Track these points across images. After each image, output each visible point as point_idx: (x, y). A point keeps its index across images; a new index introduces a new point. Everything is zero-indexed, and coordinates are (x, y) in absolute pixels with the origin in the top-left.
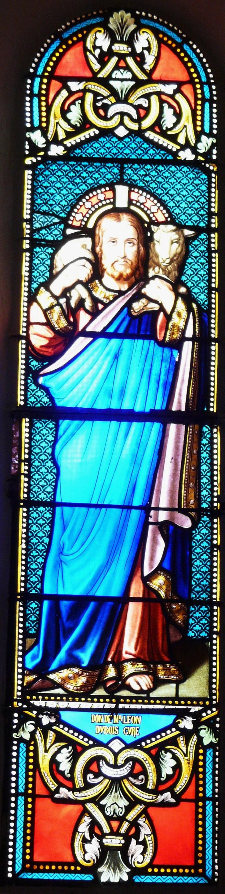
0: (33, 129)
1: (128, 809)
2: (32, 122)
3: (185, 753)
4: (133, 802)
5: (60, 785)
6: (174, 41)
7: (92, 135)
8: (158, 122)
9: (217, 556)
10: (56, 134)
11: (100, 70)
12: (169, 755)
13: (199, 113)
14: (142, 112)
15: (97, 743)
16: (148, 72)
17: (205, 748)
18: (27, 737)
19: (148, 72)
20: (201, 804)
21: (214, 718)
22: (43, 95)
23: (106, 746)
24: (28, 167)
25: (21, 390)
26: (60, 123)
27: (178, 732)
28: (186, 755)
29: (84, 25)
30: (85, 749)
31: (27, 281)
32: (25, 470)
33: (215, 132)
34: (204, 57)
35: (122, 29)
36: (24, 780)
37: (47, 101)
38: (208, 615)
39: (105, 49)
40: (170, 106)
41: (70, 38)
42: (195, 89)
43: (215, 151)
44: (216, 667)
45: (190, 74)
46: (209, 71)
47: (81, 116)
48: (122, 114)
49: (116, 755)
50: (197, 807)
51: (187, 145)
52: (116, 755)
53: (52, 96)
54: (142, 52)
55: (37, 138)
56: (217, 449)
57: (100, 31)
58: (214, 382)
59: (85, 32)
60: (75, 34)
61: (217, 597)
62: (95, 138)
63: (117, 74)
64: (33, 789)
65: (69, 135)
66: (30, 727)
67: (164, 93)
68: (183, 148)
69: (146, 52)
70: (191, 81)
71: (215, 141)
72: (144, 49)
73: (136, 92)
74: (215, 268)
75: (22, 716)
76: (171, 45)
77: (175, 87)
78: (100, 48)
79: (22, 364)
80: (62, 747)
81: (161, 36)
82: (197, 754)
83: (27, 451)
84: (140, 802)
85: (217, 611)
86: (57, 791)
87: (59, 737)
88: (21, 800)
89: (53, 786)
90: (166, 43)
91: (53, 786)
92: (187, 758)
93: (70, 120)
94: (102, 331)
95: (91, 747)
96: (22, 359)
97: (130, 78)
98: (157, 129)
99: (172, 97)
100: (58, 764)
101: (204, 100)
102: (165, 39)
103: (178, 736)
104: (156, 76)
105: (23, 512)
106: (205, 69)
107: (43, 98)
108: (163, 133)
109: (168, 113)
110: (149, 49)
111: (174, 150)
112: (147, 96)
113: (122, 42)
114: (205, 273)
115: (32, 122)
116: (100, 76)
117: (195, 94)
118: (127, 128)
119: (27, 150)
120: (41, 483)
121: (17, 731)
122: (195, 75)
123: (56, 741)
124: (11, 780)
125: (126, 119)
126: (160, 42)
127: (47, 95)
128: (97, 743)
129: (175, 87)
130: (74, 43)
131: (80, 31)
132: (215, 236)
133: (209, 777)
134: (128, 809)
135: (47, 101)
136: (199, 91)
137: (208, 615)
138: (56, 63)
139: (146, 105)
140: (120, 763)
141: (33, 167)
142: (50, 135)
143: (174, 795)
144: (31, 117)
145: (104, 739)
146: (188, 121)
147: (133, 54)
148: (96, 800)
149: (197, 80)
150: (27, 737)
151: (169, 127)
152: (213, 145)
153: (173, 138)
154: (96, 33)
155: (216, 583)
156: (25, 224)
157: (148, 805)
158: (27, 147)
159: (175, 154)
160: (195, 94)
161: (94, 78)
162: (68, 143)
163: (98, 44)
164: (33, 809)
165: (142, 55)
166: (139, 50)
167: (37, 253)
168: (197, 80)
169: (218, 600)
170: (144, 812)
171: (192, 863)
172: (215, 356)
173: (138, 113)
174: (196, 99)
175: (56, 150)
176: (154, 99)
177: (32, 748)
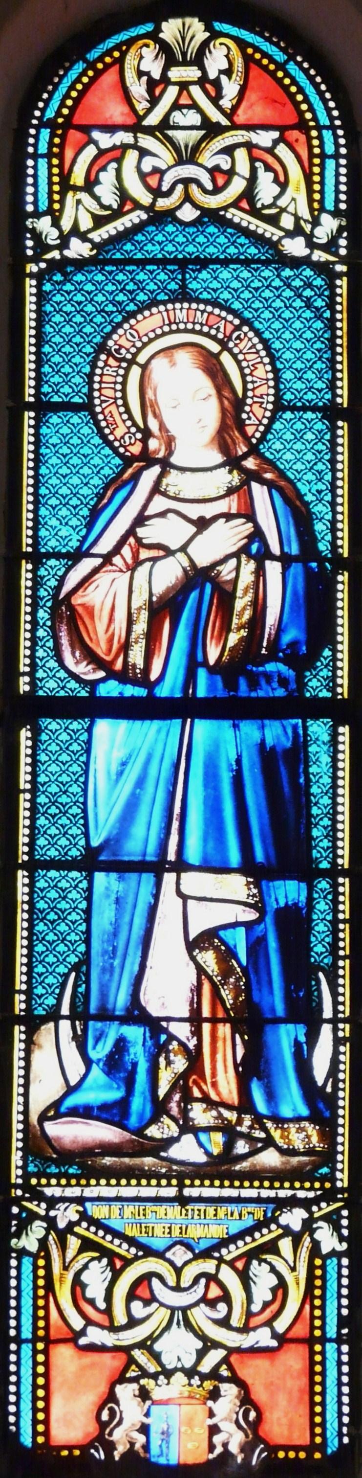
0: (37, 215)
1: (201, 1354)
2: (35, 203)
3: (292, 1265)
4: (209, 1344)
5: (89, 1322)
6: (272, 60)
7: (137, 221)
8: (249, 194)
9: (344, 968)
10: (76, 225)
11: (149, 111)
12: (265, 1267)
13: (317, 178)
14: (220, 181)
15: (149, 1252)
16: (229, 111)
17: (324, 1258)
18: (33, 1247)
19: (229, 111)
20: (318, 1348)
21: (338, 1210)
22: (55, 155)
23: (160, 1255)
24: (32, 275)
25: (26, 622)
26: (83, 200)
27: (280, 1231)
28: (293, 1269)
29: (123, 36)
30: (127, 1263)
31: (34, 362)
32: (17, 1177)
33: (343, 206)
34: (322, 83)
35: (183, 39)
36: (69, 74)
37: (61, 166)
38: (326, 336)
39: (156, 75)
40: (268, 168)
41: (100, 59)
42: (309, 139)
43: (343, 242)
44: (343, 1004)
45: (301, 113)
46: (332, 104)
47: (116, 188)
48: (186, 182)
49: (178, 1271)
50: (312, 1353)
51: (297, 231)
52: (178, 1271)
53: (69, 154)
54: (218, 78)
55: (44, 225)
56: (343, 778)
57: (147, 46)
58: (344, 1099)
59: (124, 48)
60: (109, 53)
61: (344, 862)
62: (138, 228)
63: (177, 117)
64: (47, 1328)
65: (99, 222)
66: (38, 1229)
67: (257, 146)
68: (290, 234)
69: (224, 79)
70: (302, 126)
71: (344, 223)
72: (221, 72)
73: (211, 144)
74: (344, 940)
75: (24, 1215)
76: (267, 66)
77: (276, 135)
78: (148, 74)
79: (31, 311)
80: (93, 1259)
81: (250, 51)
82: (311, 1267)
83: (24, 969)
84: (217, 1345)
85: (342, 428)
86: (83, 1333)
87: (87, 1245)
88: (26, 1349)
89: (77, 1323)
90: (258, 63)
91: (77, 1323)
92: (295, 1274)
93: (99, 197)
94: (161, 122)
95: (136, 1258)
96: (28, 528)
97: (199, 124)
98: (245, 205)
99: (270, 151)
100: (84, 1286)
101: (323, 156)
102: (258, 56)
103: (280, 1237)
104: (241, 117)
105: (20, 1032)
106: (325, 101)
107: (55, 161)
108: (255, 212)
109: (265, 179)
110: (228, 72)
111: (275, 238)
112: (229, 151)
113: (185, 63)
114: (324, 386)
115: (35, 203)
116: (146, 123)
117: (310, 147)
118: (195, 206)
119: (29, 185)
120: (74, 340)
121: (18, 1235)
122: (308, 116)
123: (81, 1251)
124: (7, 1410)
125: (194, 189)
126: (248, 60)
127: (61, 156)
128: (149, 1252)
129: (276, 135)
130: (107, 67)
131: (117, 47)
132: (345, 885)
133: (332, 1285)
134: (201, 1354)
135: (61, 166)
136: (316, 142)
137: (326, 293)
138: (77, 101)
139: (226, 166)
140: (184, 1284)
141: (40, 277)
142: (66, 224)
143: (275, 1335)
144: (35, 194)
145: (158, 1244)
146: (298, 189)
147: (203, 81)
148: (146, 1345)
149: (312, 124)
150: (33, 1247)
151: (266, 204)
152: (340, 229)
153: (273, 220)
154: (141, 48)
155: (341, 379)
156: (27, 280)
157: (231, 1351)
158: (30, 243)
159: (274, 245)
160: (310, 147)
161: (137, 127)
162: (96, 236)
163: (143, 68)
164: (46, 1364)
165: (217, 83)
166: (212, 75)
167: (41, 680)
168: (312, 124)
169: (346, 696)
170: (225, 1360)
171: (305, 1440)
172: (344, 1099)
173: (214, 180)
174: (311, 155)
175: (78, 249)
176: (241, 155)
177: (41, 1262)
